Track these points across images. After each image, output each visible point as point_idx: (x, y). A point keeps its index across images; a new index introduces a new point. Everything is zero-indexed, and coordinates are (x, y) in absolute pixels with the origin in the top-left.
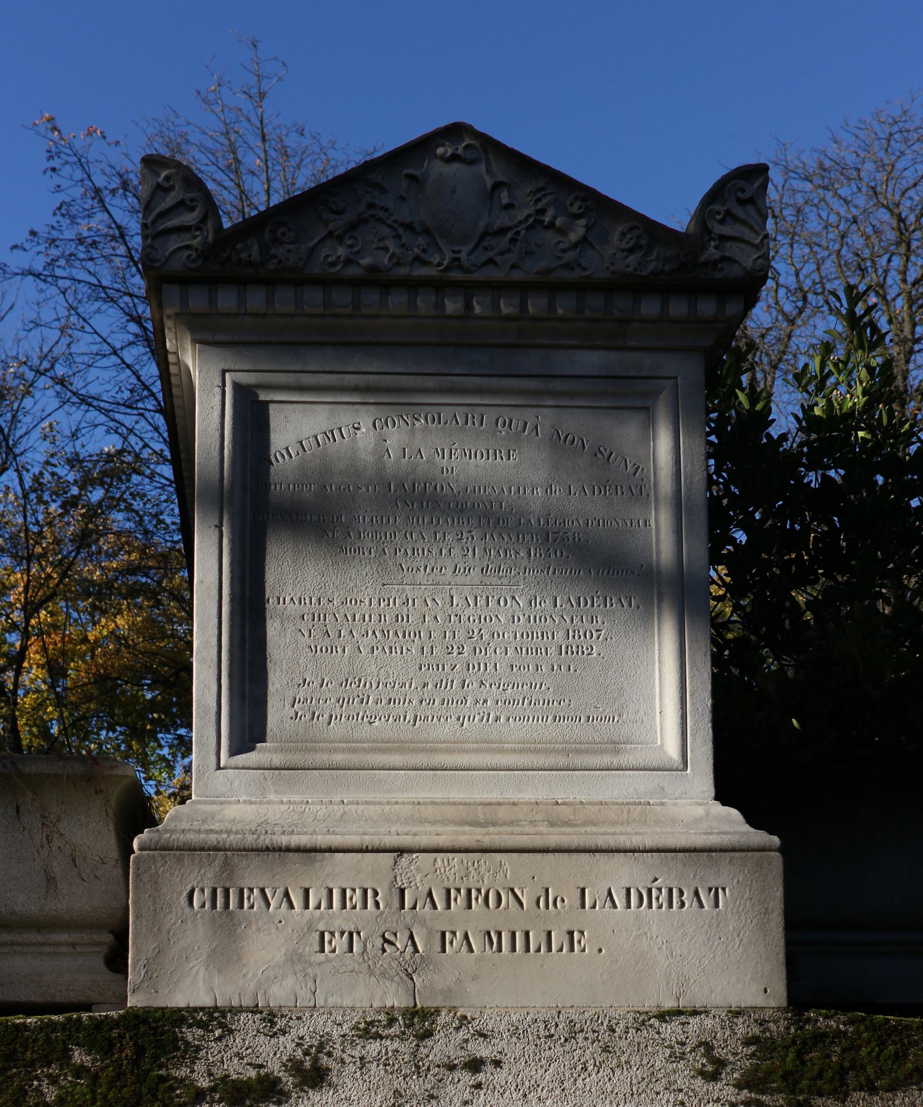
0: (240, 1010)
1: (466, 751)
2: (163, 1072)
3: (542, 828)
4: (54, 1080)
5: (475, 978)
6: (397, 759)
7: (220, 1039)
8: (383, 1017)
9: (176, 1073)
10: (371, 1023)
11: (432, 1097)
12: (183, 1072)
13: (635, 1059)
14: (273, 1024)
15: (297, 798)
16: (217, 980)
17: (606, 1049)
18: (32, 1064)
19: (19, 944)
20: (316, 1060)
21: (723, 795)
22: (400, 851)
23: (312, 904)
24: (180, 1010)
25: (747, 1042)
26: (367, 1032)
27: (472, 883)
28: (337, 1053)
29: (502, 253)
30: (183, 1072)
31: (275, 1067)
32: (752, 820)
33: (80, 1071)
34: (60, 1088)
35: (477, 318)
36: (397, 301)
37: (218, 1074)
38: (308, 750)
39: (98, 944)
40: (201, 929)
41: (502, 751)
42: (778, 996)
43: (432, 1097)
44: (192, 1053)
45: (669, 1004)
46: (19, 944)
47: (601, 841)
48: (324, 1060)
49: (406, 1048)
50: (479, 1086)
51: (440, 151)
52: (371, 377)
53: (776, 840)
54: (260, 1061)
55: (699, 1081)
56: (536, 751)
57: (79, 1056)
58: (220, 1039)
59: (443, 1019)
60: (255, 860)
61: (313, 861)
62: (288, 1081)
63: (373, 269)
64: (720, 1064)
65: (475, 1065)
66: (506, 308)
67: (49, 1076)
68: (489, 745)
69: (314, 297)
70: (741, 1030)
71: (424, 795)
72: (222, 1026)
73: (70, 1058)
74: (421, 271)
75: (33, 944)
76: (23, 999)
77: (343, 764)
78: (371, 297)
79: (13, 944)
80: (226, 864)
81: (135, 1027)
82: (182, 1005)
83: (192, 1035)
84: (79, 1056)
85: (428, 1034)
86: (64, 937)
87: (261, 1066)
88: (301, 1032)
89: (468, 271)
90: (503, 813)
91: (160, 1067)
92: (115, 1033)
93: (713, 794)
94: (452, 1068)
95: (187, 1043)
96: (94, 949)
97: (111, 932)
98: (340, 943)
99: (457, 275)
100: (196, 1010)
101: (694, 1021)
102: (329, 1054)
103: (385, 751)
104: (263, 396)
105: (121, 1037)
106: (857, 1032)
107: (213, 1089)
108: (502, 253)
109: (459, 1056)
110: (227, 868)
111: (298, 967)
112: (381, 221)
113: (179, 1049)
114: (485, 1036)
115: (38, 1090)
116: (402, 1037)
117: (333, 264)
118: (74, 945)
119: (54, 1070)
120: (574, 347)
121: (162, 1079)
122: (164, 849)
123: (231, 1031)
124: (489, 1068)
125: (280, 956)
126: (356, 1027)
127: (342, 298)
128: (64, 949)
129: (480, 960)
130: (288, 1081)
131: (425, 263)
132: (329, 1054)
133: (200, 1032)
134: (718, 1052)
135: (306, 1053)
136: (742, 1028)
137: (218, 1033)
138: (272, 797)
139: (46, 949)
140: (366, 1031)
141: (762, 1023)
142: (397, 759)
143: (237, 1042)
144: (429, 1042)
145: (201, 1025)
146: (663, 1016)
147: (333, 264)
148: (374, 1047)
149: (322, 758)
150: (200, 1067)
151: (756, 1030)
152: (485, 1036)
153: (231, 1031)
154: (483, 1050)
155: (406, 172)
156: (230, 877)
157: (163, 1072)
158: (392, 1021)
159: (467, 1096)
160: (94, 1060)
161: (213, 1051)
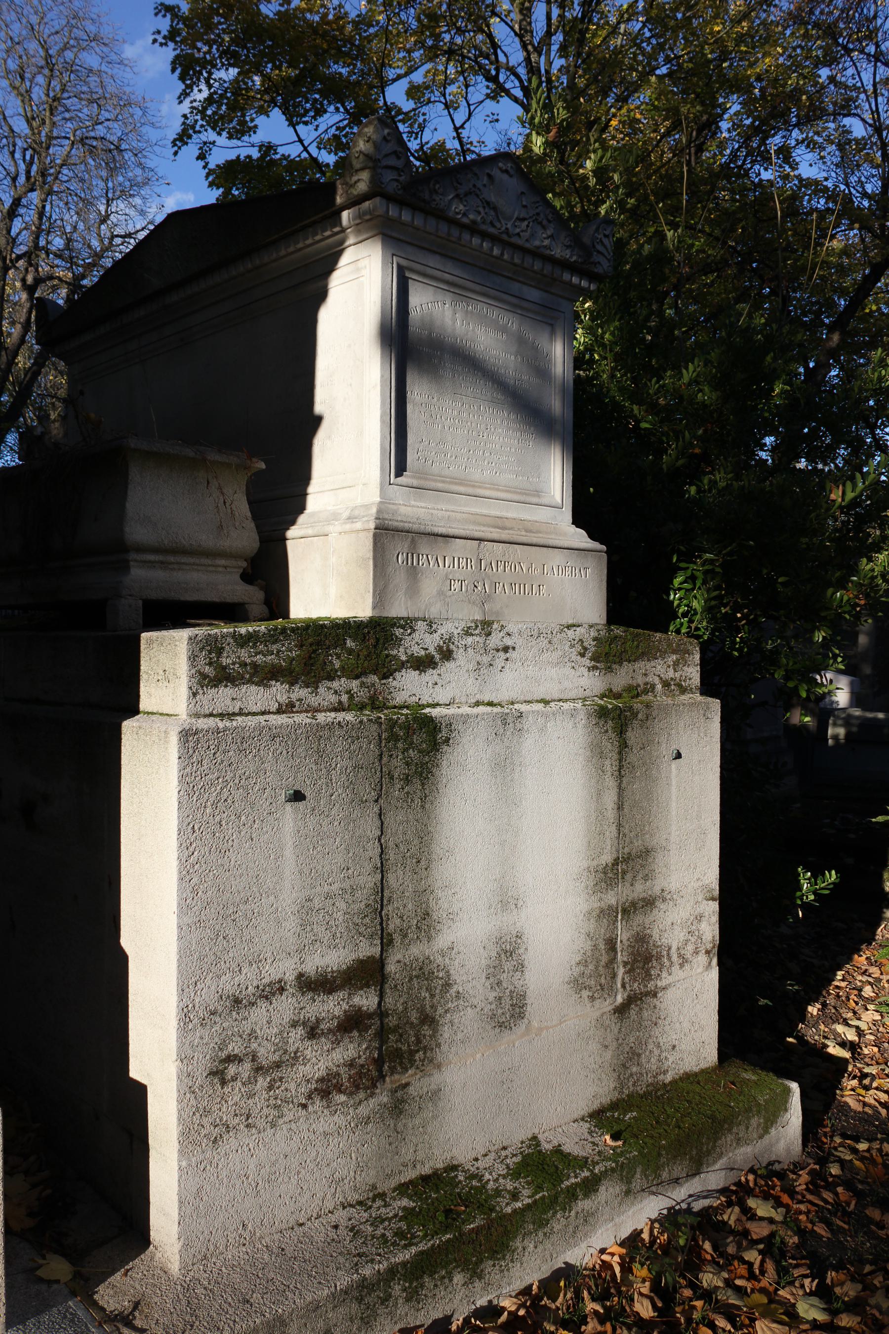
0: (417, 619)
1: (486, 488)
2: (386, 652)
3: (524, 533)
4: (338, 657)
5: (507, 606)
6: (462, 489)
7: (410, 634)
8: (473, 625)
9: (391, 652)
10: (469, 628)
11: (491, 665)
12: (394, 652)
13: (559, 647)
14: (431, 627)
15: (423, 505)
16: (409, 603)
17: (550, 642)
18: (329, 648)
19: (197, 565)
20: (448, 646)
21: (577, 521)
22: (480, 540)
23: (447, 566)
24: (394, 618)
25: (595, 639)
26: (467, 632)
27: (506, 558)
28: (456, 643)
29: (522, 231)
30: (394, 652)
31: (432, 650)
32: (592, 536)
33: (350, 652)
34: (342, 661)
35: (503, 260)
36: (476, 241)
37: (410, 653)
38: (426, 479)
39: (239, 567)
40: (402, 575)
41: (498, 490)
42: (603, 620)
43: (491, 665)
44: (398, 642)
45: (570, 622)
46: (197, 565)
47: (535, 540)
48: (452, 647)
49: (481, 640)
50: (507, 659)
51: (500, 165)
52: (455, 278)
53: (604, 548)
54: (426, 647)
55: (579, 657)
56: (515, 492)
57: (350, 643)
58: (410, 634)
59: (495, 626)
60: (425, 539)
61: (448, 542)
62: (437, 657)
63: (474, 222)
64: (585, 649)
65: (506, 649)
66: (517, 260)
67: (336, 654)
68: (495, 486)
69: (444, 227)
70: (592, 634)
71: (473, 510)
72: (411, 627)
73: (345, 644)
74: (492, 230)
75: (205, 565)
76: (209, 599)
77: (441, 489)
78: (466, 236)
79: (194, 564)
80: (413, 540)
81: (375, 627)
82: (395, 616)
83: (398, 632)
84: (350, 643)
85: (489, 634)
86: (223, 562)
87: (427, 649)
88: (443, 631)
89: (510, 236)
90: (508, 524)
91: (386, 649)
92: (366, 630)
93: (571, 521)
94: (498, 650)
95: (396, 636)
96: (236, 570)
97: (245, 560)
98: (456, 585)
99: (505, 237)
100: (401, 618)
101: (578, 629)
102: (453, 643)
103: (456, 484)
104: (408, 274)
105: (369, 632)
106: (626, 636)
107: (407, 661)
108: (522, 231)
109: (500, 645)
110: (413, 545)
111: (442, 598)
112: (477, 196)
113: (392, 639)
114: (509, 635)
115: (331, 662)
116: (479, 635)
117: (457, 213)
118: (226, 567)
119: (338, 651)
120: (531, 286)
121: (387, 656)
122: (386, 529)
123: (414, 630)
124: (510, 650)
125: (435, 592)
126: (463, 630)
127: (455, 232)
128: (220, 569)
129: (509, 597)
130: (437, 657)
131: (494, 226)
132: (453, 643)
133: (402, 631)
134: (585, 644)
135: (444, 643)
136: (593, 634)
137: (409, 631)
138: (413, 503)
139: (211, 569)
140: (467, 631)
141: (598, 631)
142: (462, 489)
143: (416, 636)
144: (490, 638)
145: (403, 627)
146: (569, 627)
147: (457, 213)
148: (470, 640)
149: (433, 485)
150: (402, 649)
151: (596, 634)
152: (509, 635)
153: (414, 630)
154: (509, 642)
155: (487, 171)
156: (414, 548)
157: (386, 652)
158: (477, 626)
159: (503, 665)
160: (357, 645)
161: (407, 641)
